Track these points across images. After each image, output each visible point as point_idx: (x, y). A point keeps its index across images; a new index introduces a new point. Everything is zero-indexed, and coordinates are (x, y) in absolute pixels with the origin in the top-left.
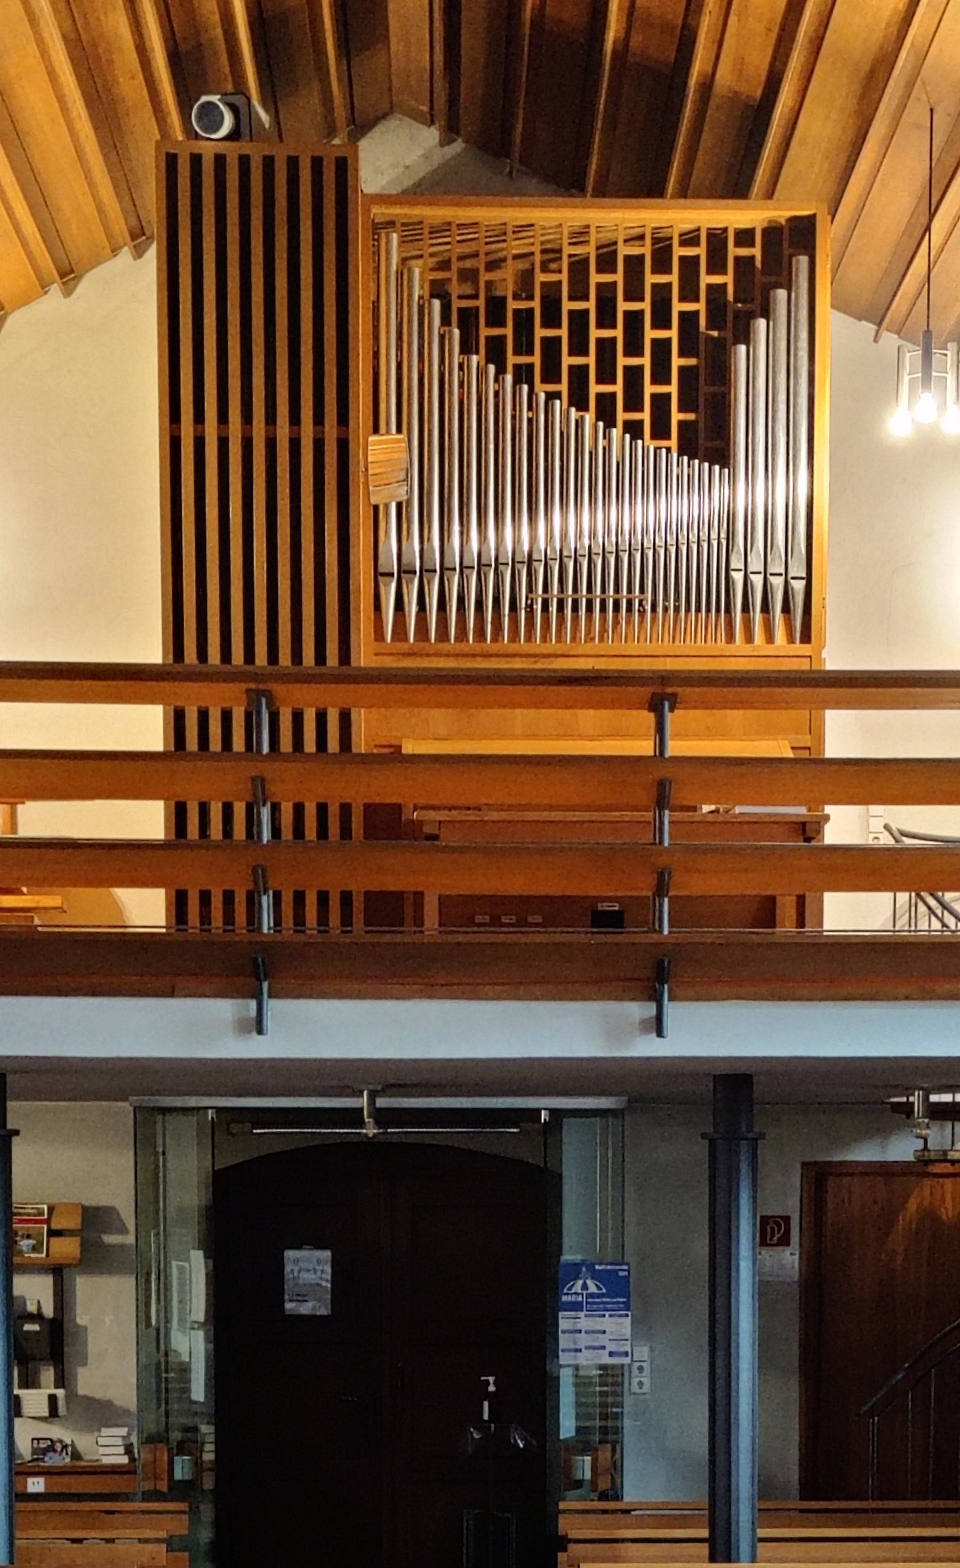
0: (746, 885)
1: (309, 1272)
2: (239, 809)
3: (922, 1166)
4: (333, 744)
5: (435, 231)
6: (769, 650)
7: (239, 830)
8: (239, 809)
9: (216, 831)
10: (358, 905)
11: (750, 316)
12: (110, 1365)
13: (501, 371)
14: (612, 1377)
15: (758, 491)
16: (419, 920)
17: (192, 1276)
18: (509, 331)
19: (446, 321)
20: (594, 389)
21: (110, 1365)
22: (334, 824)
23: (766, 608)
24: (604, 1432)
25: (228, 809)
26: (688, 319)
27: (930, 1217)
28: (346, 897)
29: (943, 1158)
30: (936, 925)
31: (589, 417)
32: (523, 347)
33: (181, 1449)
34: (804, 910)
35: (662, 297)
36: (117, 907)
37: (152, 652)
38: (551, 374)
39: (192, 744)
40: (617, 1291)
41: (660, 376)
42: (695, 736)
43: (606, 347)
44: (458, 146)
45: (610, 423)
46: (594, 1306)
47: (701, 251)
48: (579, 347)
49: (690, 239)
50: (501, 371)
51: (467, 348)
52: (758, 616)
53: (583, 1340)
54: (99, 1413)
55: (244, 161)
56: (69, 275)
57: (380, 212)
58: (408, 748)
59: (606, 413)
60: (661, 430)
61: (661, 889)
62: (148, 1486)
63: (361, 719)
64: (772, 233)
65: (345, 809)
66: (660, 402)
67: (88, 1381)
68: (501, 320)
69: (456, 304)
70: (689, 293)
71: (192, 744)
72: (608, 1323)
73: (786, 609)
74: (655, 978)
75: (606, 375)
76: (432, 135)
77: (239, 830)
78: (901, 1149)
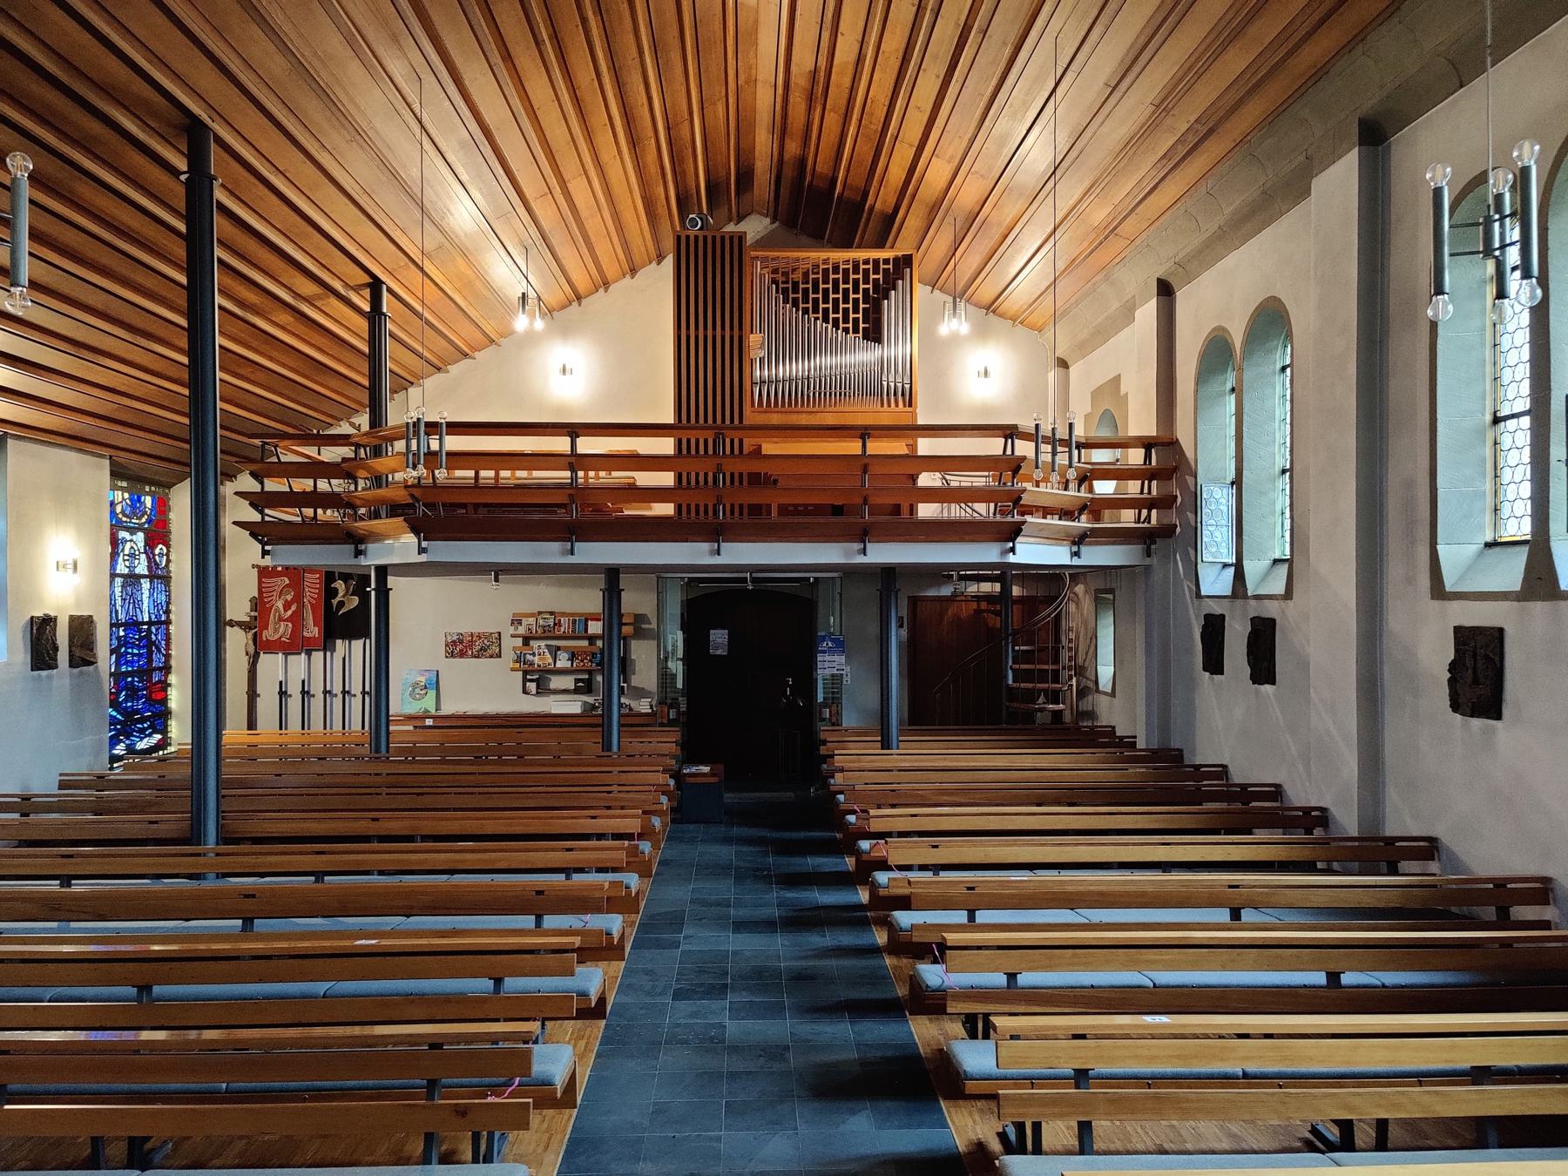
0: (890, 500)
1: (719, 638)
3: (953, 598)
10: (745, 511)
12: (645, 674)
14: (836, 680)
15: (895, 349)
16: (770, 513)
17: (675, 639)
21: (645, 674)
24: (834, 700)
26: (866, 291)
28: (741, 506)
33: (671, 707)
34: (912, 510)
37: (669, 418)
38: (816, 311)
39: (685, 451)
40: (840, 646)
41: (856, 311)
42: (876, 447)
43: (836, 301)
46: (831, 651)
48: (826, 301)
49: (866, 262)
51: (786, 301)
54: (640, 693)
55: (705, 238)
56: (633, 271)
59: (836, 324)
60: (856, 331)
63: (746, 441)
64: (896, 259)
65: (741, 475)
66: (856, 321)
67: (635, 681)
68: (799, 291)
70: (866, 281)
71: (685, 451)
72: (836, 658)
74: (863, 535)
75: (836, 311)
76: (768, 220)
78: (946, 591)
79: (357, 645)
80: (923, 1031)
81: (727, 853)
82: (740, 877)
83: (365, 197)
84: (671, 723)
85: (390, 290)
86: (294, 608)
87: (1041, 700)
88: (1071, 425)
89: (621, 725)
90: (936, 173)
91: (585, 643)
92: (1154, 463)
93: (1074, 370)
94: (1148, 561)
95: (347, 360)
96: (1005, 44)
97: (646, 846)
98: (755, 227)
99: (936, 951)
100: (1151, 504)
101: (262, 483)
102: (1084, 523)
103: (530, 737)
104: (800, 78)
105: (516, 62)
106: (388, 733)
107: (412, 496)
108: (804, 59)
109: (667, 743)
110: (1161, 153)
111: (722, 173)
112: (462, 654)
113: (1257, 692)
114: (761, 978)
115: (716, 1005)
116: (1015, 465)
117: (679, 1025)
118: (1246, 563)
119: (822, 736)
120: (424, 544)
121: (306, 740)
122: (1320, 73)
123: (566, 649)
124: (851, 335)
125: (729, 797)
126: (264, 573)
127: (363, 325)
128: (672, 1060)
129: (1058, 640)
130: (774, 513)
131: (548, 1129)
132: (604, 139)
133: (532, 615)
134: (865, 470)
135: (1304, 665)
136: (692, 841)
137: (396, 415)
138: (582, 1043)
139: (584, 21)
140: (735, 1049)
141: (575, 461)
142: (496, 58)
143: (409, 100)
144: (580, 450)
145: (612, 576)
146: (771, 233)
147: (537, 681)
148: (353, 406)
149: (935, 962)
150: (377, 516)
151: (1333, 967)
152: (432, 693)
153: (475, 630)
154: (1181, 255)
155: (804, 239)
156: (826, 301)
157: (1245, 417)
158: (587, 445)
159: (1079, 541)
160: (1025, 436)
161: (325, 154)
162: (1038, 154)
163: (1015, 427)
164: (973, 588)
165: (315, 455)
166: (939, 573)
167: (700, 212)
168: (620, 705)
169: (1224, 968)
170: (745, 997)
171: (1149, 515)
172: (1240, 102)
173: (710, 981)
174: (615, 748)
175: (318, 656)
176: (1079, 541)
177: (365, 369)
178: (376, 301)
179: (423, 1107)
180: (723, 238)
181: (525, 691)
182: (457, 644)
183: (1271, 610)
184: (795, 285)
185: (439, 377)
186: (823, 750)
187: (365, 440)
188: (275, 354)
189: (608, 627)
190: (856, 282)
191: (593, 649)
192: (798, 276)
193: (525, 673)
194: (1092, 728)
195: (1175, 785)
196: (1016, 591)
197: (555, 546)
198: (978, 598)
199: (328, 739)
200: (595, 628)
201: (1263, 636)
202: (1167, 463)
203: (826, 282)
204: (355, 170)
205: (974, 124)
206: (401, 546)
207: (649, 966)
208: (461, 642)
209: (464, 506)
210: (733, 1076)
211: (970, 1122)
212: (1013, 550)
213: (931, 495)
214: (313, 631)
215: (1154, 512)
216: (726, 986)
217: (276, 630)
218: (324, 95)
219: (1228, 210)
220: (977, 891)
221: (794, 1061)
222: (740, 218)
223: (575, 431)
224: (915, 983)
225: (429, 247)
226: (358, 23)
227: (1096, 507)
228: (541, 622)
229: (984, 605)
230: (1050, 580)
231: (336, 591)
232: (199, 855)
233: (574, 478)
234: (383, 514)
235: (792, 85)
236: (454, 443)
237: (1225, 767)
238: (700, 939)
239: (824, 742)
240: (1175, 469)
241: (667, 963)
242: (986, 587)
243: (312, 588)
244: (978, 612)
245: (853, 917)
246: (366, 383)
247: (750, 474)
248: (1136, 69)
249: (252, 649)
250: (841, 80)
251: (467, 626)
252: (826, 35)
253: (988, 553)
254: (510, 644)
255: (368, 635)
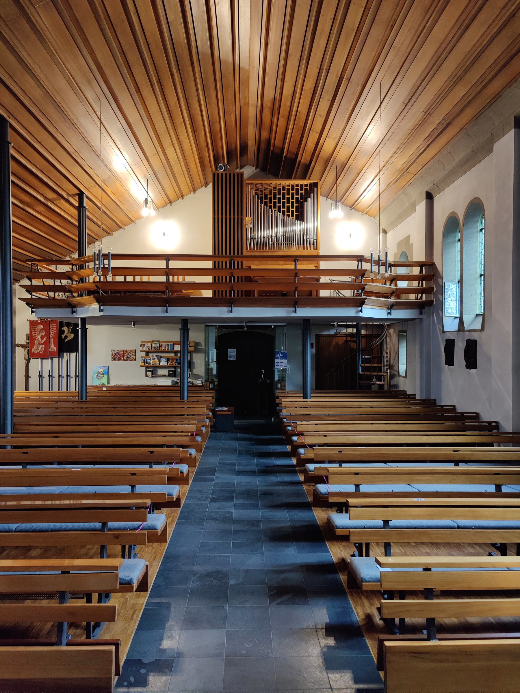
0: (308, 289)
1: (232, 353)
2: (228, 277)
4: (240, 267)
5: (256, 184)
6: (311, 251)
7: (228, 281)
8: (228, 277)
9: (224, 281)
10: (243, 292)
11: (307, 198)
12: (199, 369)
13: (267, 207)
14: (284, 371)
15: (310, 225)
16: (254, 295)
17: (213, 354)
18: (268, 200)
19: (258, 199)
20: (282, 209)
21: (199, 369)
22: (240, 280)
23: (310, 244)
24: (283, 380)
25: (226, 277)
26: (297, 198)
27: (337, 344)
28: (242, 291)
29: (339, 333)
30: (338, 295)
31: (281, 214)
32: (270, 203)
33: (211, 383)
34: (317, 293)
35: (293, 195)
36: (201, 293)
38: (275, 207)
39: (217, 267)
40: (285, 356)
41: (293, 207)
43: (284, 203)
44: (258, 170)
45: (284, 215)
46: (281, 358)
47: (299, 187)
48: (279, 203)
49: (297, 185)
50: (267, 207)
51: (261, 203)
52: (309, 246)
53: (279, 364)
54: (197, 377)
56: (195, 191)
57: (248, 182)
58: (252, 267)
59: (284, 213)
60: (293, 216)
61: (296, 290)
62: (206, 389)
63: (244, 263)
64: (310, 184)
65: (242, 277)
66: (293, 211)
67: (195, 371)
68: (268, 199)
69: (260, 196)
70: (297, 194)
71: (217, 267)
72: (283, 361)
73: (313, 244)
74: (295, 304)
75: (284, 207)
76: (254, 168)
77: (228, 281)
78: (332, 332)
79: (73, 355)
80: (319, 515)
81: (235, 444)
82: (240, 454)
83: (76, 154)
84: (211, 389)
85: (87, 197)
86: (45, 339)
87: (374, 380)
88: (386, 253)
89: (188, 390)
90: (328, 146)
91: (173, 355)
92: (424, 273)
93: (389, 234)
94: (421, 317)
95: (69, 229)
96: (358, 85)
97: (199, 438)
98: (248, 171)
99: (323, 479)
100: (422, 291)
101: (31, 281)
102: (393, 300)
103: (148, 394)
104: (268, 103)
105: (142, 93)
106: (86, 393)
107: (97, 286)
108: (269, 94)
109: (209, 397)
110: (428, 134)
111: (233, 146)
112: (119, 359)
113: (468, 372)
114: (249, 494)
115: (229, 504)
116: (362, 273)
117: (211, 512)
118: (464, 316)
119: (277, 395)
120: (102, 308)
121: (51, 395)
122: (497, 96)
123: (165, 357)
124: (290, 218)
125: (236, 422)
126: (32, 323)
127: (75, 212)
128: (207, 526)
129: (381, 353)
130: (256, 294)
131: (155, 552)
132: (181, 130)
133: (149, 342)
134: (296, 275)
135: (489, 359)
136: (220, 439)
137: (89, 251)
138: (170, 519)
139: (172, 75)
140: (237, 522)
141: (168, 272)
142: (133, 91)
143: (95, 110)
144: (171, 266)
145: (185, 324)
146: (256, 173)
147: (152, 371)
148: (71, 250)
149: (325, 484)
150: (81, 295)
151: (498, 483)
152: (106, 377)
153: (125, 349)
154: (436, 181)
155: (270, 176)
156: (279, 203)
157: (464, 252)
158: (174, 264)
159: (391, 307)
160: (366, 261)
161: (59, 134)
162: (372, 135)
163: (362, 256)
164: (344, 331)
165: (54, 269)
166: (328, 322)
167: (224, 163)
168: (188, 382)
169: (450, 483)
170: (241, 501)
171: (422, 297)
172: (462, 110)
173: (227, 495)
174: (186, 398)
175: (56, 360)
176: (391, 307)
177: (76, 233)
178: (81, 202)
179: (100, 534)
180: (234, 175)
181: (147, 376)
182: (115, 355)
183: (475, 336)
184: (266, 196)
185: (109, 237)
186: (278, 401)
187: (76, 262)
188: (37, 225)
189: (183, 348)
190: (293, 194)
191: (176, 357)
192: (267, 192)
193: (147, 367)
194: (396, 392)
195: (432, 412)
196: (363, 332)
197: (160, 309)
198: (346, 335)
199: (60, 395)
200: (177, 348)
201: (471, 348)
202: (430, 274)
203: (279, 194)
204: (73, 142)
205: (345, 122)
206: (92, 309)
207: (200, 489)
208: (118, 354)
209: (120, 292)
210: (236, 532)
211: (339, 551)
212: (361, 311)
213: (326, 286)
214: (54, 349)
215: (424, 295)
216: (233, 497)
217: (38, 348)
218: (58, 107)
219: (457, 160)
220: (343, 452)
221: (262, 526)
222: (242, 167)
223: (168, 258)
224: (317, 495)
225: (104, 177)
226: (74, 77)
227: (397, 293)
228: (154, 345)
229: (349, 338)
230: (378, 328)
231: (64, 331)
232: (4, 438)
233: (168, 279)
234: (84, 294)
235: (264, 104)
236: (116, 263)
237: (454, 406)
238: (223, 478)
239: (278, 397)
240: (433, 276)
241: (208, 488)
242: (350, 330)
243: (54, 328)
244: (346, 341)
245: (290, 470)
246: (77, 239)
247: (245, 291)
248: (416, 95)
249: (27, 357)
250: (286, 103)
251: (134, 476)
252: (279, 82)
253: (350, 312)
254: (140, 355)
255: (77, 351)
